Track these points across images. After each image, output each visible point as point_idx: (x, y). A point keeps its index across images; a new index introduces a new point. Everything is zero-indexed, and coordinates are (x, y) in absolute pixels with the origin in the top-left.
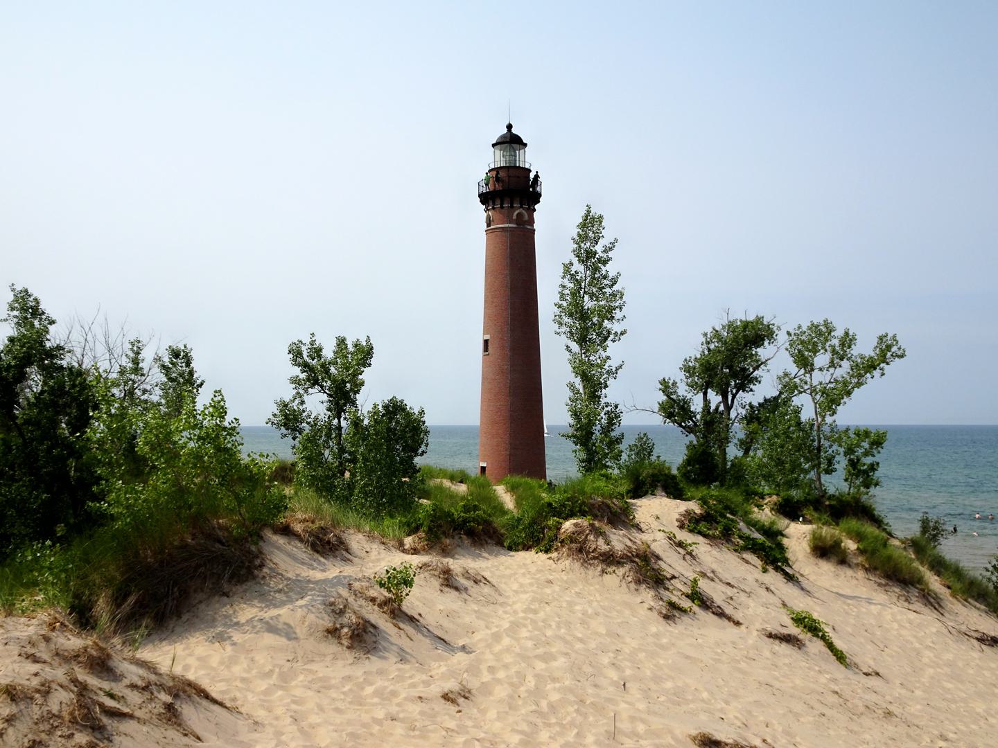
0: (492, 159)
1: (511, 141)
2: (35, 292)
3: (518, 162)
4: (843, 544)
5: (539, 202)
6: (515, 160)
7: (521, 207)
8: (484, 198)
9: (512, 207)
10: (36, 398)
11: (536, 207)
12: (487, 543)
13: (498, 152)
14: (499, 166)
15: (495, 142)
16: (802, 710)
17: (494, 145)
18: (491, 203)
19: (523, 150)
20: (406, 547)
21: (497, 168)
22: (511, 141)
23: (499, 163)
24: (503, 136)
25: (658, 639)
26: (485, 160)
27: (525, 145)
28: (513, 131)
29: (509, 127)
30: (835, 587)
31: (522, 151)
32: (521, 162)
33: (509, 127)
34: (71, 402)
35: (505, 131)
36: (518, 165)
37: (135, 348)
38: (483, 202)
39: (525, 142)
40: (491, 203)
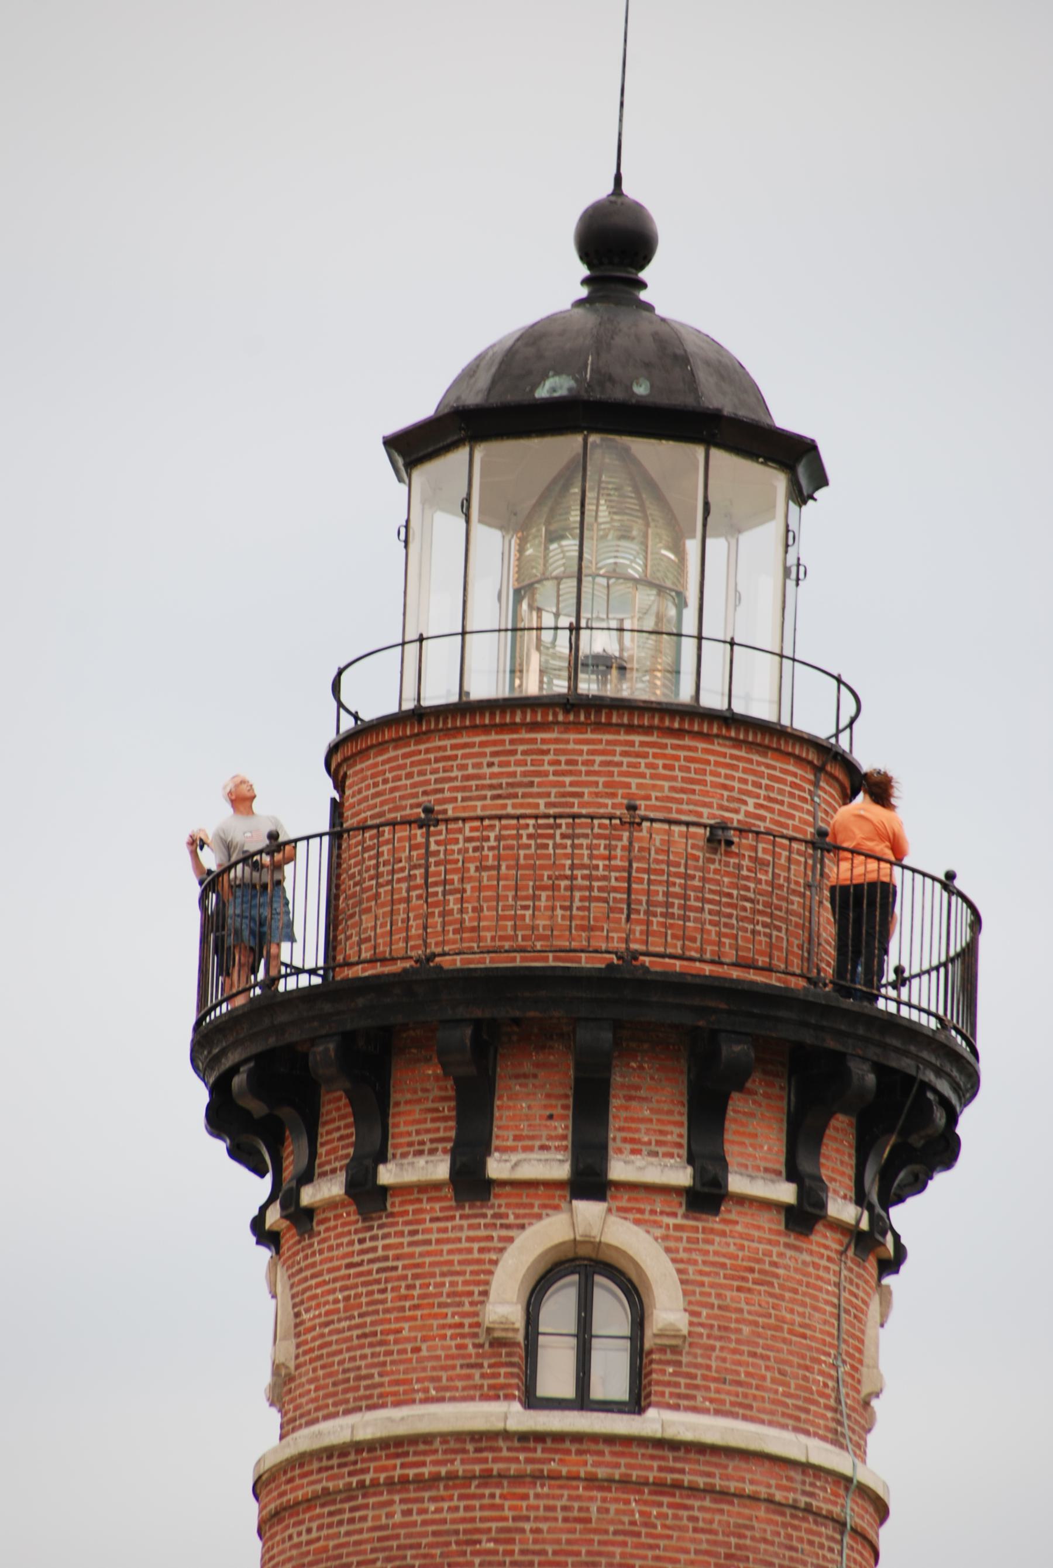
1: (605, 396)
5: (945, 1151)
7: (589, 1182)
8: (302, 1069)
9: (470, 1183)
15: (421, 406)
17: (411, 448)
18: (338, 1133)
22: (605, 396)
24: (530, 351)
27: (796, 461)
28: (667, 287)
29: (615, 245)
33: (615, 245)
35: (560, 282)
39: (787, 416)
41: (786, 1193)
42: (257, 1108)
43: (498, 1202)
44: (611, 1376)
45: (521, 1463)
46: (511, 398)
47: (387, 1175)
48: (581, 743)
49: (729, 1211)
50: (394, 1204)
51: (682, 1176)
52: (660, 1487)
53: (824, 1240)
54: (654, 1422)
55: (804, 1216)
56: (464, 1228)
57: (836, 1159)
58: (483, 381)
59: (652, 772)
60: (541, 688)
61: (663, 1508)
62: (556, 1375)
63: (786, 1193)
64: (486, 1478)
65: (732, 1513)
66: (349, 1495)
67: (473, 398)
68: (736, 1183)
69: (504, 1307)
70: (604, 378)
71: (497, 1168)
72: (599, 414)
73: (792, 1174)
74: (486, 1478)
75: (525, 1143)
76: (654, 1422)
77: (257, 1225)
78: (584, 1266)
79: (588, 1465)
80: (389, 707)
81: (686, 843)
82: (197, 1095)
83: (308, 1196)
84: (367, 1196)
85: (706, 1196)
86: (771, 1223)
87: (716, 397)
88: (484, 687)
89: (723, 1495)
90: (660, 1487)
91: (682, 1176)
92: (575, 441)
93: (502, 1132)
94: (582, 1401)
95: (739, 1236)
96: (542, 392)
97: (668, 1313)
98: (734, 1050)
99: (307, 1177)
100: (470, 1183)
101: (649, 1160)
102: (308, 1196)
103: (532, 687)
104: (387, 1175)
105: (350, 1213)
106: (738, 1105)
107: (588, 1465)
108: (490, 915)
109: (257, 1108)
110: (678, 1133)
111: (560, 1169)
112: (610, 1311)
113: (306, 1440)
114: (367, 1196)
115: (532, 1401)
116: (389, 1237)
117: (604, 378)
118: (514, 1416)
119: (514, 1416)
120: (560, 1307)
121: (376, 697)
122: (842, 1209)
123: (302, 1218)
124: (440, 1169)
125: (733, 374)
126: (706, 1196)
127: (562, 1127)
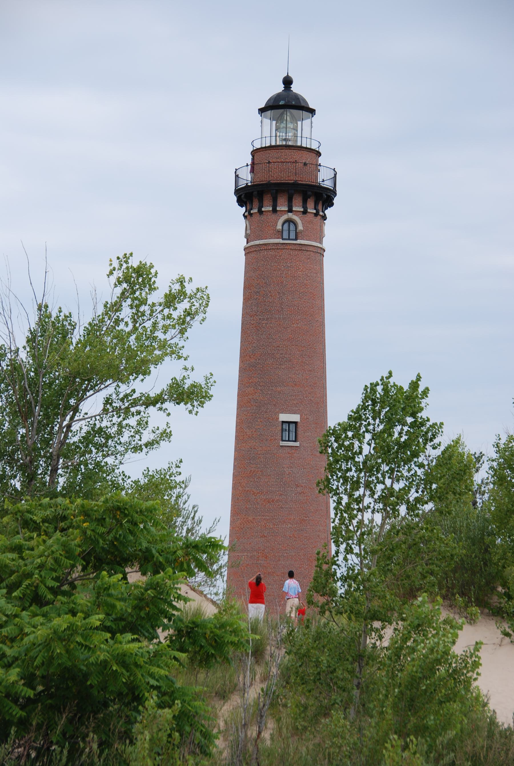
1: (286, 104)
3: (299, 139)
5: (332, 205)
6: (296, 136)
7: (290, 210)
8: (245, 196)
9: (275, 211)
10: (252, 203)
12: (187, 615)
13: (267, 122)
14: (268, 145)
15: (263, 106)
16: (379, 606)
17: (262, 111)
18: (256, 203)
19: (309, 120)
20: (19, 703)
22: (286, 104)
23: (268, 139)
24: (277, 97)
26: (238, 137)
27: (312, 112)
28: (295, 88)
29: (288, 82)
30: (154, 678)
32: (304, 140)
33: (288, 82)
35: (280, 88)
36: (299, 144)
38: (241, 202)
39: (311, 106)
40: (256, 203)
41: (315, 211)
42: (245, 200)
43: (278, 213)
44: (293, 236)
45: (282, 247)
46: (276, 104)
47: (263, 209)
48: (287, 151)
49: (308, 214)
50: (264, 213)
51: (302, 210)
52: (299, 250)
53: (319, 217)
54: (299, 242)
55: (316, 214)
56: (274, 216)
57: (320, 207)
58: (272, 101)
59: (296, 155)
60: (276, 143)
61: (300, 253)
62: (285, 235)
63: (315, 211)
64: (277, 249)
65: (309, 253)
66: (259, 250)
67: (271, 104)
68: (309, 210)
69: (279, 227)
70: (289, 101)
71: (278, 209)
72: (288, 106)
73: (315, 209)
74: (277, 249)
75: (282, 205)
76: (299, 242)
77: (244, 215)
78: (289, 221)
79: (291, 247)
80: (259, 147)
81: (302, 165)
82: (235, 198)
83: (252, 212)
84: (260, 212)
85: (305, 212)
86: (313, 215)
87: (303, 104)
88: (273, 144)
89: (307, 251)
90: (299, 250)
91: (302, 210)
92: (282, 110)
93: (278, 204)
94: (289, 239)
95: (309, 217)
96: (280, 104)
97: (300, 227)
98: (309, 193)
99: (251, 209)
100: (275, 211)
101: (282, 207)
102: (252, 212)
103: (278, 144)
104: (263, 209)
105: (258, 214)
106: (309, 200)
107: (291, 247)
108: (279, 175)
109: (245, 200)
110: (301, 204)
111: (286, 209)
112: (292, 227)
113: (250, 244)
114: (260, 212)
115: (283, 239)
116: (263, 217)
117: (289, 101)
118: (280, 241)
119: (280, 241)
120: (286, 226)
121: (258, 146)
122: (321, 213)
123: (251, 214)
124: (271, 209)
125: (304, 100)
126: (305, 212)
127: (287, 203)
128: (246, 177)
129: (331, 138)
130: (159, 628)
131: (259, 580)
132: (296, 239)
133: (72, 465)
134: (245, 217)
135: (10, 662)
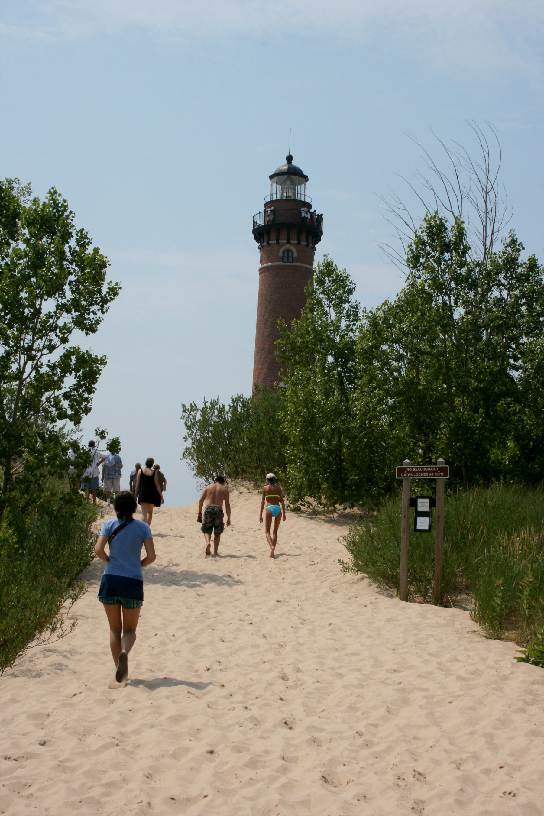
0: (270, 191)
1: (291, 175)
2: (122, 445)
4: (61, 404)
5: (320, 240)
7: (288, 242)
8: (260, 234)
11: (316, 246)
15: (272, 173)
17: (271, 177)
21: (277, 201)
22: (291, 175)
25: (150, 487)
26: (256, 196)
28: (295, 163)
29: (289, 159)
31: (303, 186)
33: (289, 159)
34: (511, 325)
37: (379, 522)
39: (305, 173)
44: (290, 260)
47: (270, 242)
60: (282, 196)
62: (285, 260)
71: (280, 241)
82: (253, 236)
94: (288, 262)
111: (285, 241)
115: (283, 262)
119: (282, 263)
128: (261, 221)
129: (316, 195)
130: (200, 420)
131: (339, 560)
132: (293, 262)
133: (503, 337)
134: (259, 248)
135: (273, 235)
